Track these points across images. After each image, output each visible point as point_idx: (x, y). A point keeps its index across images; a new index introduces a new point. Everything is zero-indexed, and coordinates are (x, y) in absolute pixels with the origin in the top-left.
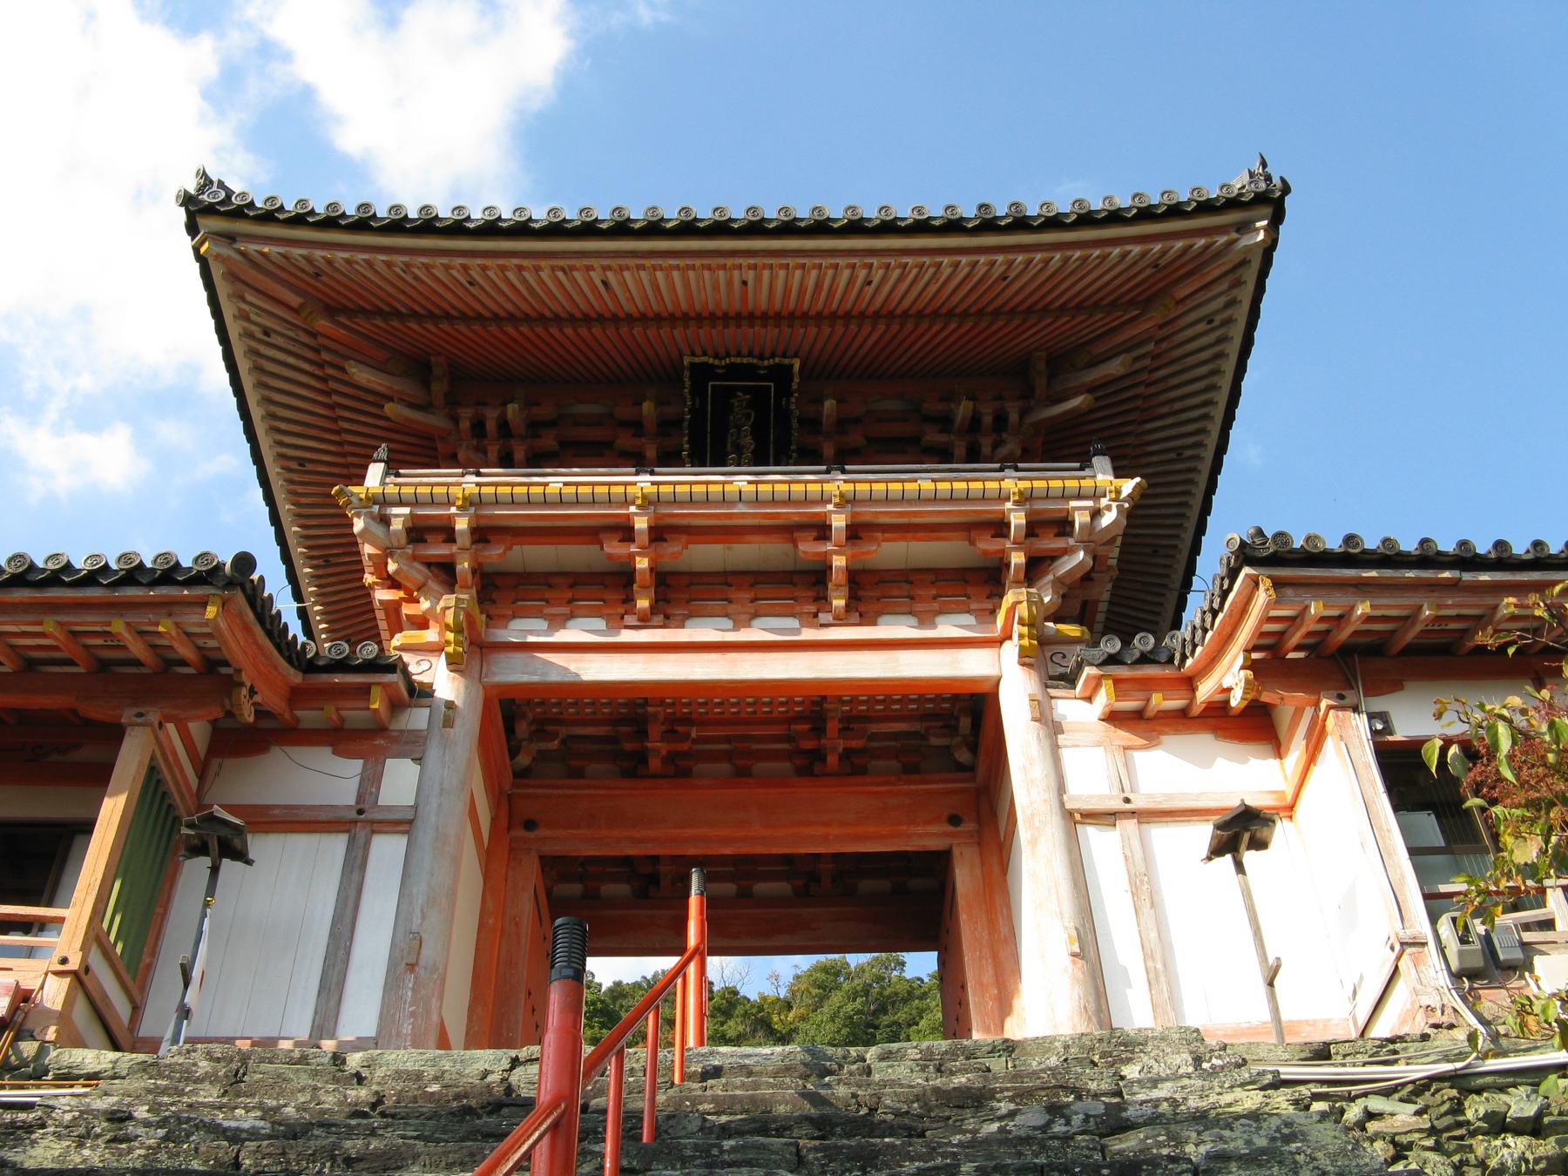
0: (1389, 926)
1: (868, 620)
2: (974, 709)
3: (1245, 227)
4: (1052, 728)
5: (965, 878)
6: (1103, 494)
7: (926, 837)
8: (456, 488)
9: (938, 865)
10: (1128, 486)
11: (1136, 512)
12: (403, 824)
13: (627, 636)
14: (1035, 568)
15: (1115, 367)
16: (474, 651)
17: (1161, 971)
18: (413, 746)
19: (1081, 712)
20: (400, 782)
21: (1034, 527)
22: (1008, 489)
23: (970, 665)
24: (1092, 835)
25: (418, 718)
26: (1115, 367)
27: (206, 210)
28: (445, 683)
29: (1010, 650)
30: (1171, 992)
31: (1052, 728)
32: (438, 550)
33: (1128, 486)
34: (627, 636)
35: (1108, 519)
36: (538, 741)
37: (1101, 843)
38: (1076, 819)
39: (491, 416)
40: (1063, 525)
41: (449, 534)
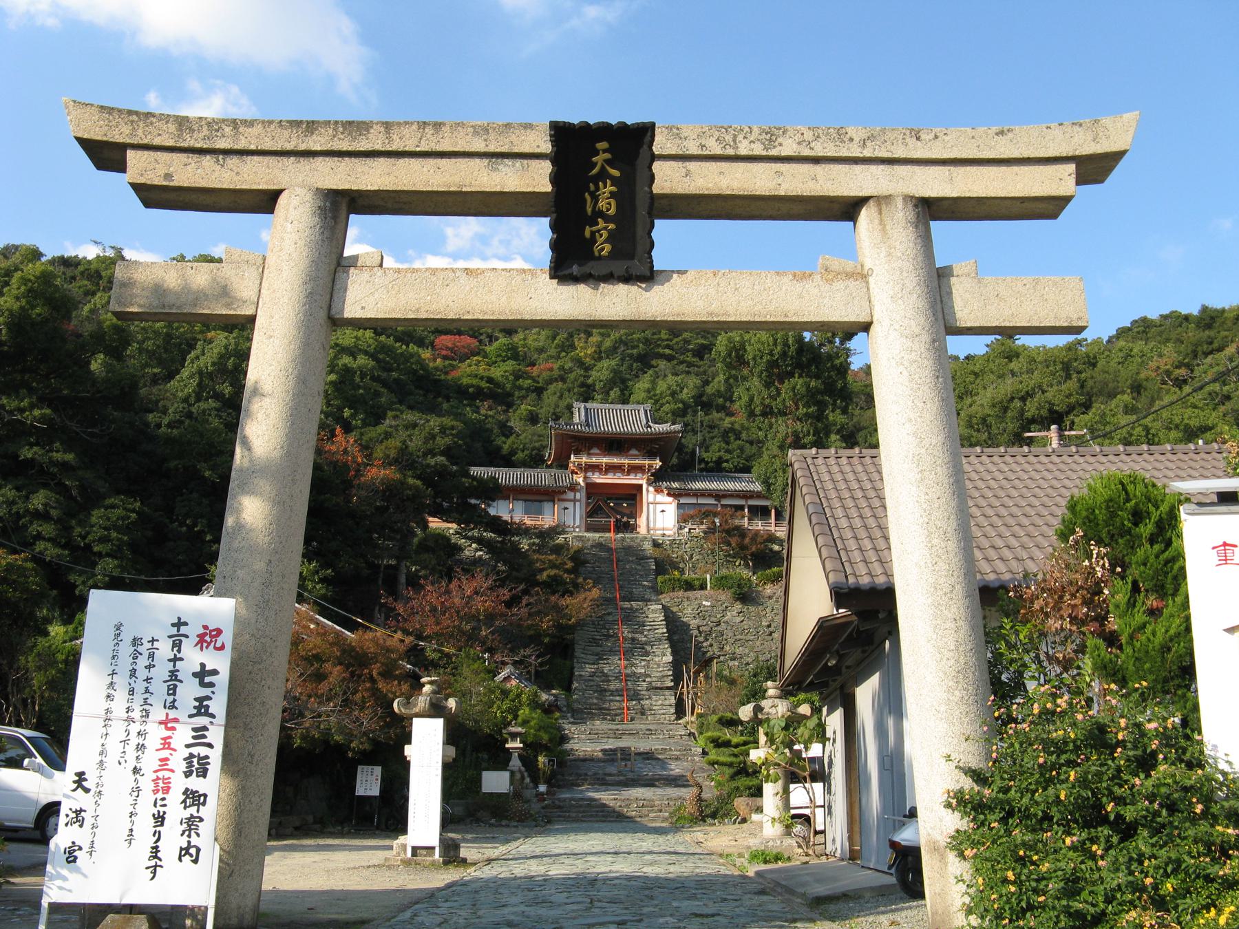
8: (584, 459)
16: (585, 478)
18: (579, 491)
19: (651, 489)
23: (640, 482)
28: (582, 484)
36: (591, 488)
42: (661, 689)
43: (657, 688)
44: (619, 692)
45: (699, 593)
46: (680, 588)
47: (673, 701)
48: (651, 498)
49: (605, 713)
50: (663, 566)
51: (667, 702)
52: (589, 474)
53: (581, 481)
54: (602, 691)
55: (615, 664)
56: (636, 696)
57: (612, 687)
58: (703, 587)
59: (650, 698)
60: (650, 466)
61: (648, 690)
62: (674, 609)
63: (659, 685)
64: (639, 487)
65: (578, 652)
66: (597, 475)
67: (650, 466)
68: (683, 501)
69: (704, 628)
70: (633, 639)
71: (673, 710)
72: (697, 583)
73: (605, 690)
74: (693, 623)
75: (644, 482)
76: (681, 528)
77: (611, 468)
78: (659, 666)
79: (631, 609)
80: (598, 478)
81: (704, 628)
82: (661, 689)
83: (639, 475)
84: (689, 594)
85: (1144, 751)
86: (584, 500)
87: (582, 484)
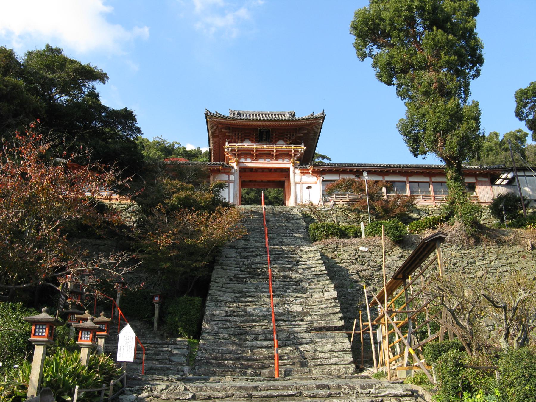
0: (319, 198)
1: (277, 160)
2: (287, 170)
3: (320, 120)
4: (294, 173)
5: (286, 184)
6: (302, 148)
7: (282, 179)
8: (237, 146)
9: (284, 182)
10: (305, 148)
11: (305, 151)
12: (233, 182)
13: (253, 162)
14: (295, 155)
15: (306, 132)
16: (238, 163)
17: (302, 197)
18: (233, 174)
19: (298, 171)
20: (232, 178)
21: (295, 151)
22: (293, 147)
23: (287, 166)
24: (297, 185)
25: (233, 171)
26: (306, 132)
27: (209, 116)
28: (236, 167)
29: (292, 164)
30: (351, 172)
31: (294, 173)
32: (234, 152)
33: (305, 148)
34: (253, 162)
35: (302, 151)
36: (244, 171)
37: (298, 185)
38: (295, 183)
39: (237, 133)
40: (298, 151)
41: (235, 150)
42: (328, 329)
43: (320, 329)
44: (267, 336)
45: (354, 240)
46: (334, 234)
47: (347, 344)
48: (298, 179)
49: (244, 365)
50: (312, 226)
51: (338, 347)
52: (242, 160)
53: (234, 165)
54: (242, 334)
55: (263, 303)
56: (291, 340)
57: (257, 329)
58: (357, 234)
59: (312, 342)
60: (296, 151)
61: (308, 331)
62: (330, 255)
63: (323, 324)
64: (287, 170)
65: (214, 290)
66: (248, 160)
67: (296, 151)
68: (327, 177)
69: (365, 273)
70: (285, 277)
71: (349, 358)
72: (351, 231)
73: (247, 333)
74: (352, 268)
75: (290, 166)
76: (326, 201)
77: (261, 154)
78: (320, 302)
79: (283, 250)
80: (250, 163)
81: (365, 273)
82: (328, 329)
83: (286, 161)
84: (346, 240)
85: (81, 380)
86: (237, 181)
87: (236, 167)
